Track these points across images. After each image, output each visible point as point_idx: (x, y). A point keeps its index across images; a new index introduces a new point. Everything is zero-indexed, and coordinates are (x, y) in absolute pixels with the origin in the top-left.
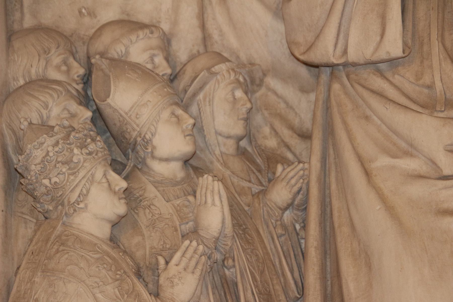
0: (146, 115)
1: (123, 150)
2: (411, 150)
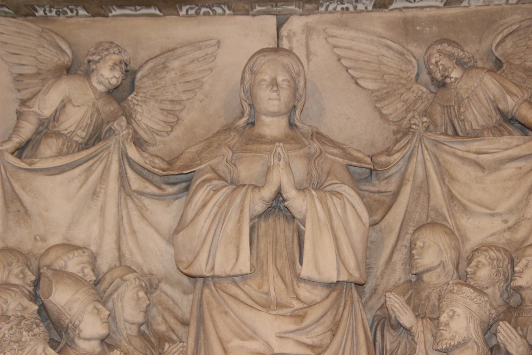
0: (76, 308)
2: (253, 336)
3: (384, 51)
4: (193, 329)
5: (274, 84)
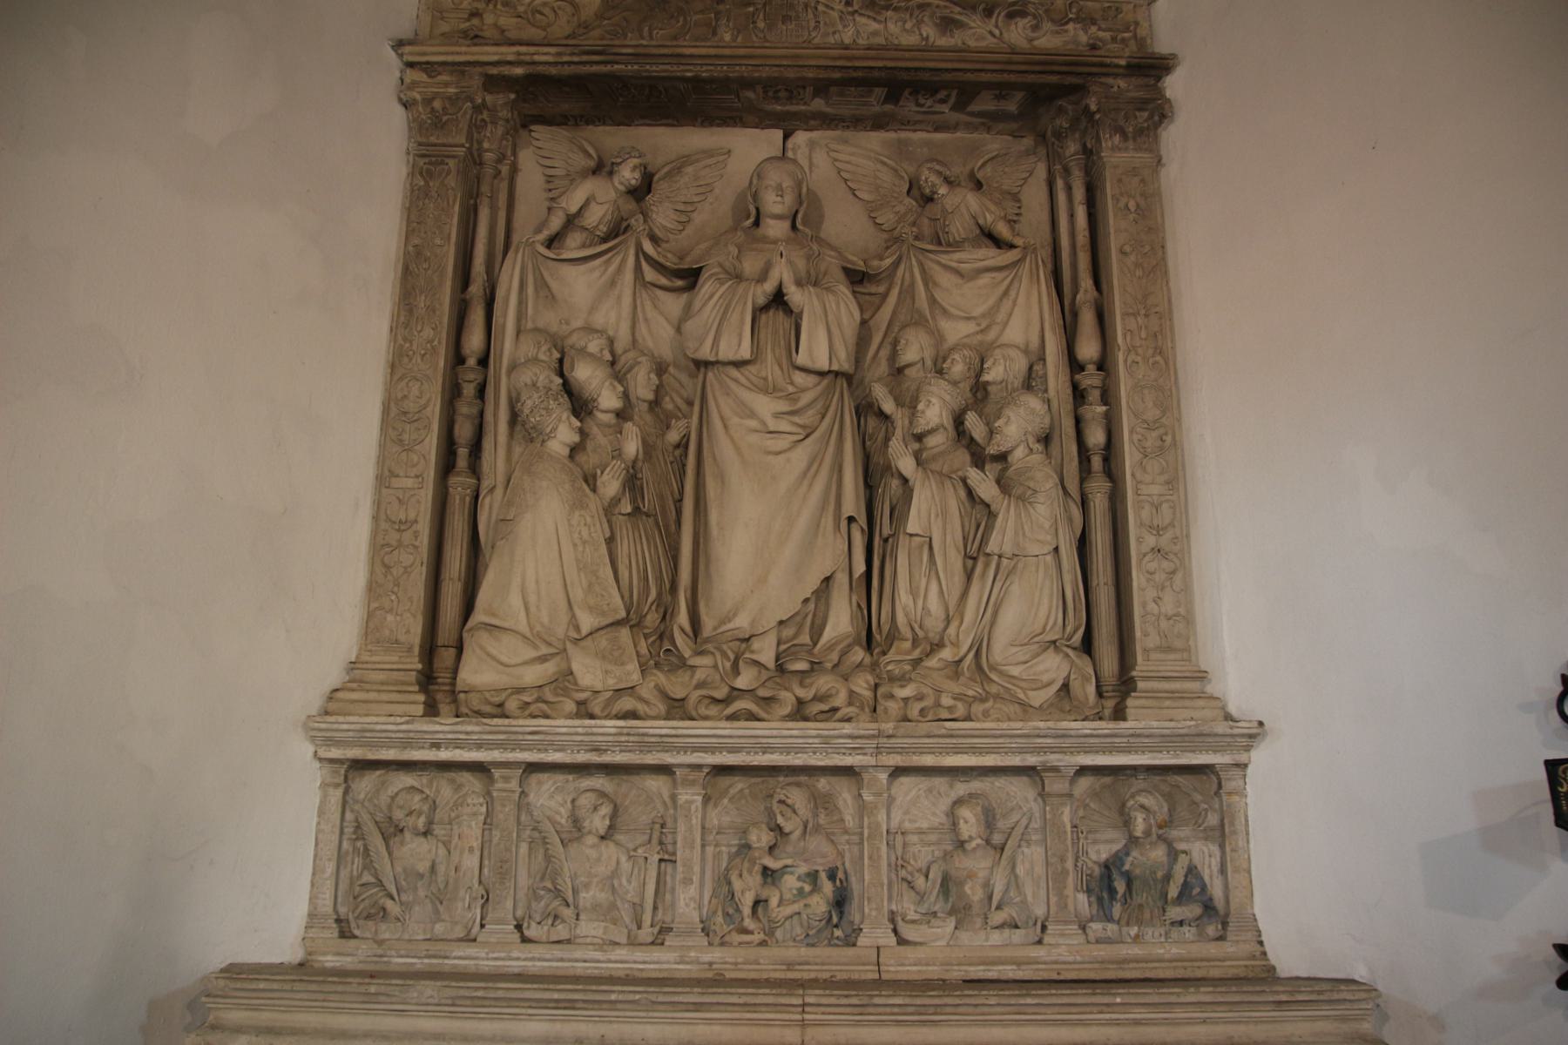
0: (595, 383)
1: (580, 406)
2: (752, 414)
3: (879, 166)
4: (696, 408)
5: (780, 191)
